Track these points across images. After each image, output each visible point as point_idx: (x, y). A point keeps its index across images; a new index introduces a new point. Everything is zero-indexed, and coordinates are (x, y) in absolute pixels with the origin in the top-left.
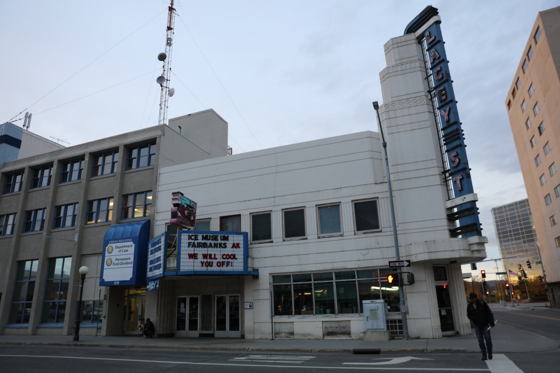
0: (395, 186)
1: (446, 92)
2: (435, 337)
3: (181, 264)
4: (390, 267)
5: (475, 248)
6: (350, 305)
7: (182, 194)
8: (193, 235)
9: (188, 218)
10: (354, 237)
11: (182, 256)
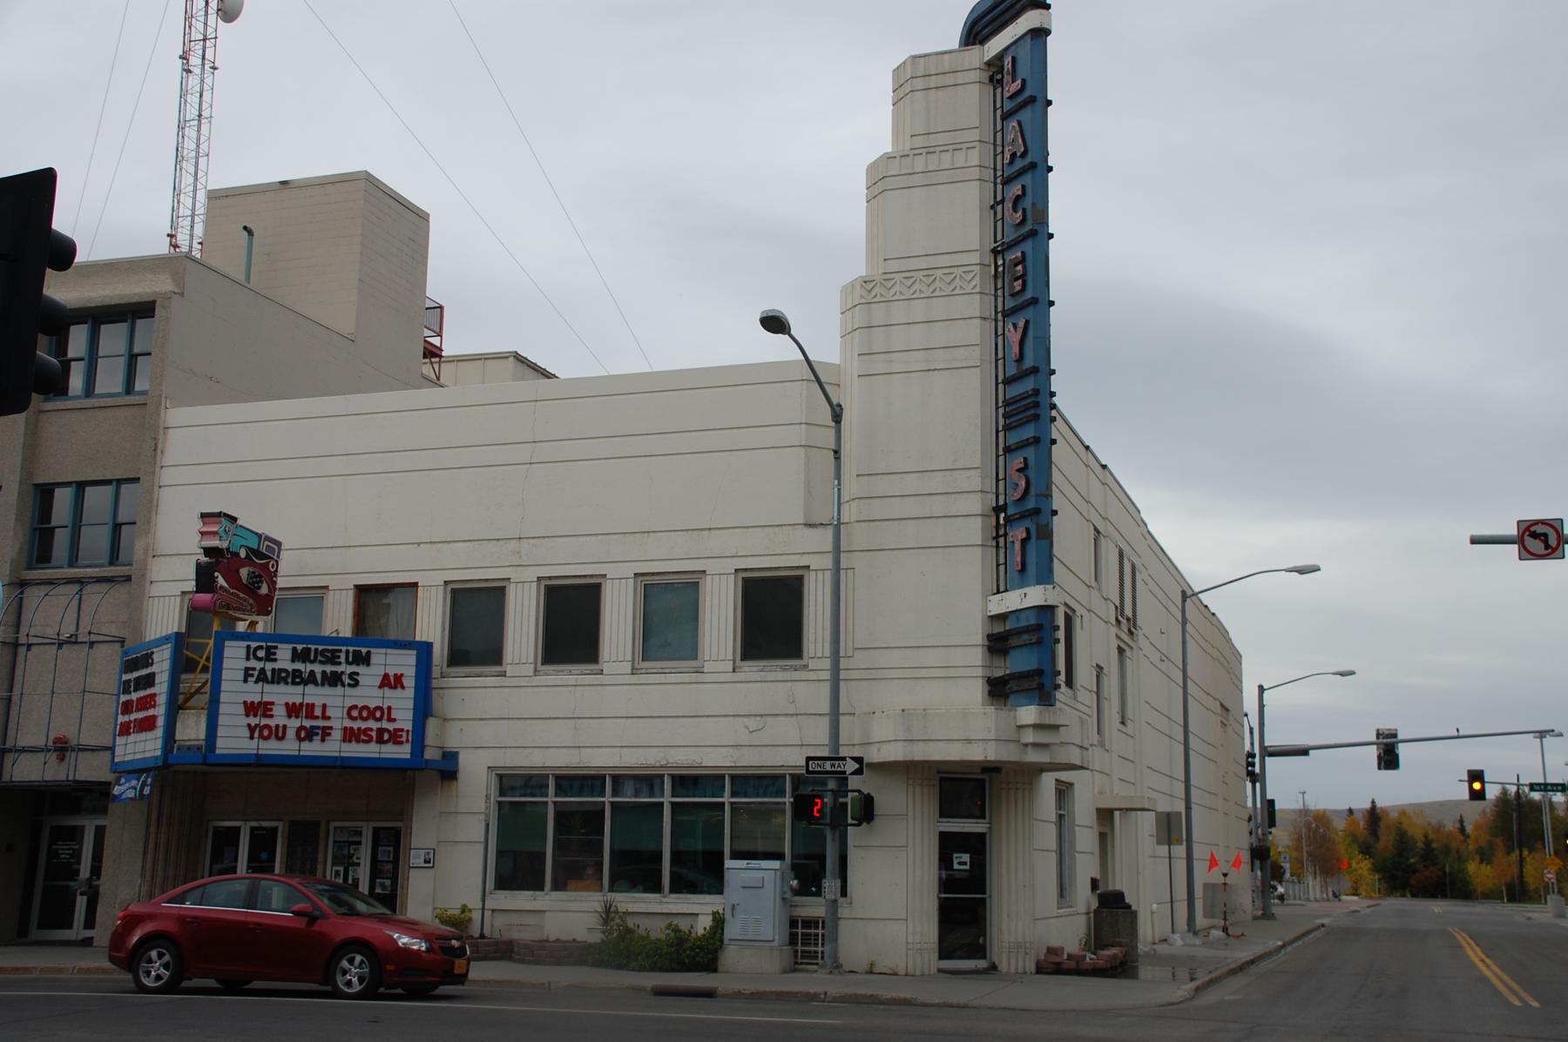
0: (855, 537)
1: (1025, 268)
2: (910, 971)
3: (221, 732)
4: (808, 772)
5: (1029, 737)
6: (701, 872)
7: (234, 519)
8: (260, 647)
9: (251, 589)
10: (729, 677)
11: (223, 709)
